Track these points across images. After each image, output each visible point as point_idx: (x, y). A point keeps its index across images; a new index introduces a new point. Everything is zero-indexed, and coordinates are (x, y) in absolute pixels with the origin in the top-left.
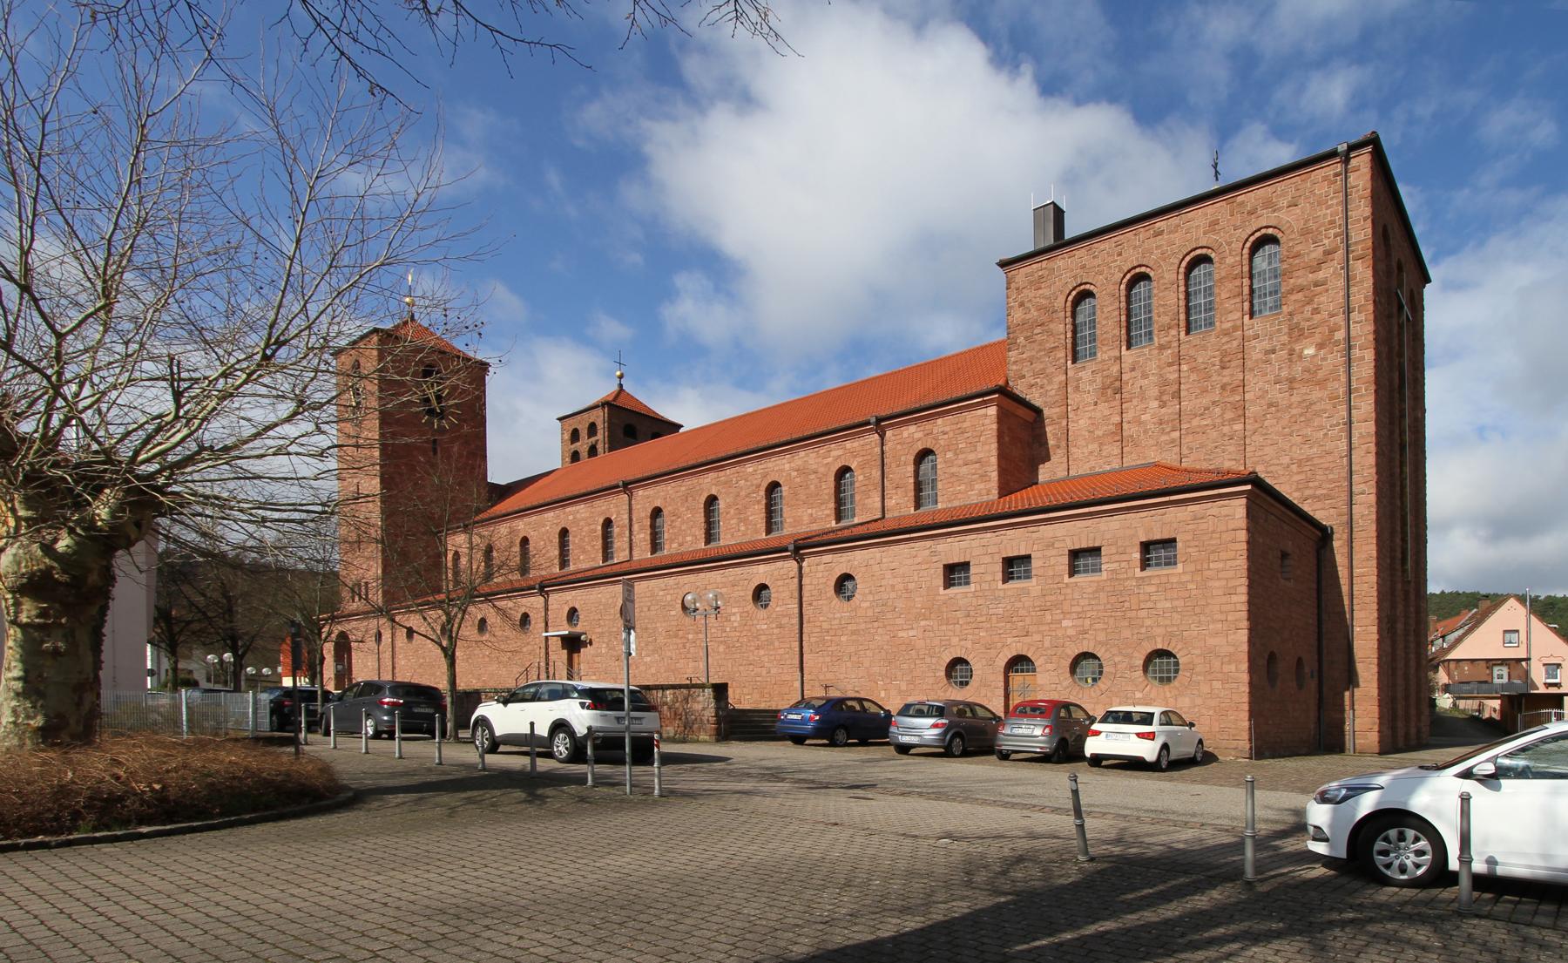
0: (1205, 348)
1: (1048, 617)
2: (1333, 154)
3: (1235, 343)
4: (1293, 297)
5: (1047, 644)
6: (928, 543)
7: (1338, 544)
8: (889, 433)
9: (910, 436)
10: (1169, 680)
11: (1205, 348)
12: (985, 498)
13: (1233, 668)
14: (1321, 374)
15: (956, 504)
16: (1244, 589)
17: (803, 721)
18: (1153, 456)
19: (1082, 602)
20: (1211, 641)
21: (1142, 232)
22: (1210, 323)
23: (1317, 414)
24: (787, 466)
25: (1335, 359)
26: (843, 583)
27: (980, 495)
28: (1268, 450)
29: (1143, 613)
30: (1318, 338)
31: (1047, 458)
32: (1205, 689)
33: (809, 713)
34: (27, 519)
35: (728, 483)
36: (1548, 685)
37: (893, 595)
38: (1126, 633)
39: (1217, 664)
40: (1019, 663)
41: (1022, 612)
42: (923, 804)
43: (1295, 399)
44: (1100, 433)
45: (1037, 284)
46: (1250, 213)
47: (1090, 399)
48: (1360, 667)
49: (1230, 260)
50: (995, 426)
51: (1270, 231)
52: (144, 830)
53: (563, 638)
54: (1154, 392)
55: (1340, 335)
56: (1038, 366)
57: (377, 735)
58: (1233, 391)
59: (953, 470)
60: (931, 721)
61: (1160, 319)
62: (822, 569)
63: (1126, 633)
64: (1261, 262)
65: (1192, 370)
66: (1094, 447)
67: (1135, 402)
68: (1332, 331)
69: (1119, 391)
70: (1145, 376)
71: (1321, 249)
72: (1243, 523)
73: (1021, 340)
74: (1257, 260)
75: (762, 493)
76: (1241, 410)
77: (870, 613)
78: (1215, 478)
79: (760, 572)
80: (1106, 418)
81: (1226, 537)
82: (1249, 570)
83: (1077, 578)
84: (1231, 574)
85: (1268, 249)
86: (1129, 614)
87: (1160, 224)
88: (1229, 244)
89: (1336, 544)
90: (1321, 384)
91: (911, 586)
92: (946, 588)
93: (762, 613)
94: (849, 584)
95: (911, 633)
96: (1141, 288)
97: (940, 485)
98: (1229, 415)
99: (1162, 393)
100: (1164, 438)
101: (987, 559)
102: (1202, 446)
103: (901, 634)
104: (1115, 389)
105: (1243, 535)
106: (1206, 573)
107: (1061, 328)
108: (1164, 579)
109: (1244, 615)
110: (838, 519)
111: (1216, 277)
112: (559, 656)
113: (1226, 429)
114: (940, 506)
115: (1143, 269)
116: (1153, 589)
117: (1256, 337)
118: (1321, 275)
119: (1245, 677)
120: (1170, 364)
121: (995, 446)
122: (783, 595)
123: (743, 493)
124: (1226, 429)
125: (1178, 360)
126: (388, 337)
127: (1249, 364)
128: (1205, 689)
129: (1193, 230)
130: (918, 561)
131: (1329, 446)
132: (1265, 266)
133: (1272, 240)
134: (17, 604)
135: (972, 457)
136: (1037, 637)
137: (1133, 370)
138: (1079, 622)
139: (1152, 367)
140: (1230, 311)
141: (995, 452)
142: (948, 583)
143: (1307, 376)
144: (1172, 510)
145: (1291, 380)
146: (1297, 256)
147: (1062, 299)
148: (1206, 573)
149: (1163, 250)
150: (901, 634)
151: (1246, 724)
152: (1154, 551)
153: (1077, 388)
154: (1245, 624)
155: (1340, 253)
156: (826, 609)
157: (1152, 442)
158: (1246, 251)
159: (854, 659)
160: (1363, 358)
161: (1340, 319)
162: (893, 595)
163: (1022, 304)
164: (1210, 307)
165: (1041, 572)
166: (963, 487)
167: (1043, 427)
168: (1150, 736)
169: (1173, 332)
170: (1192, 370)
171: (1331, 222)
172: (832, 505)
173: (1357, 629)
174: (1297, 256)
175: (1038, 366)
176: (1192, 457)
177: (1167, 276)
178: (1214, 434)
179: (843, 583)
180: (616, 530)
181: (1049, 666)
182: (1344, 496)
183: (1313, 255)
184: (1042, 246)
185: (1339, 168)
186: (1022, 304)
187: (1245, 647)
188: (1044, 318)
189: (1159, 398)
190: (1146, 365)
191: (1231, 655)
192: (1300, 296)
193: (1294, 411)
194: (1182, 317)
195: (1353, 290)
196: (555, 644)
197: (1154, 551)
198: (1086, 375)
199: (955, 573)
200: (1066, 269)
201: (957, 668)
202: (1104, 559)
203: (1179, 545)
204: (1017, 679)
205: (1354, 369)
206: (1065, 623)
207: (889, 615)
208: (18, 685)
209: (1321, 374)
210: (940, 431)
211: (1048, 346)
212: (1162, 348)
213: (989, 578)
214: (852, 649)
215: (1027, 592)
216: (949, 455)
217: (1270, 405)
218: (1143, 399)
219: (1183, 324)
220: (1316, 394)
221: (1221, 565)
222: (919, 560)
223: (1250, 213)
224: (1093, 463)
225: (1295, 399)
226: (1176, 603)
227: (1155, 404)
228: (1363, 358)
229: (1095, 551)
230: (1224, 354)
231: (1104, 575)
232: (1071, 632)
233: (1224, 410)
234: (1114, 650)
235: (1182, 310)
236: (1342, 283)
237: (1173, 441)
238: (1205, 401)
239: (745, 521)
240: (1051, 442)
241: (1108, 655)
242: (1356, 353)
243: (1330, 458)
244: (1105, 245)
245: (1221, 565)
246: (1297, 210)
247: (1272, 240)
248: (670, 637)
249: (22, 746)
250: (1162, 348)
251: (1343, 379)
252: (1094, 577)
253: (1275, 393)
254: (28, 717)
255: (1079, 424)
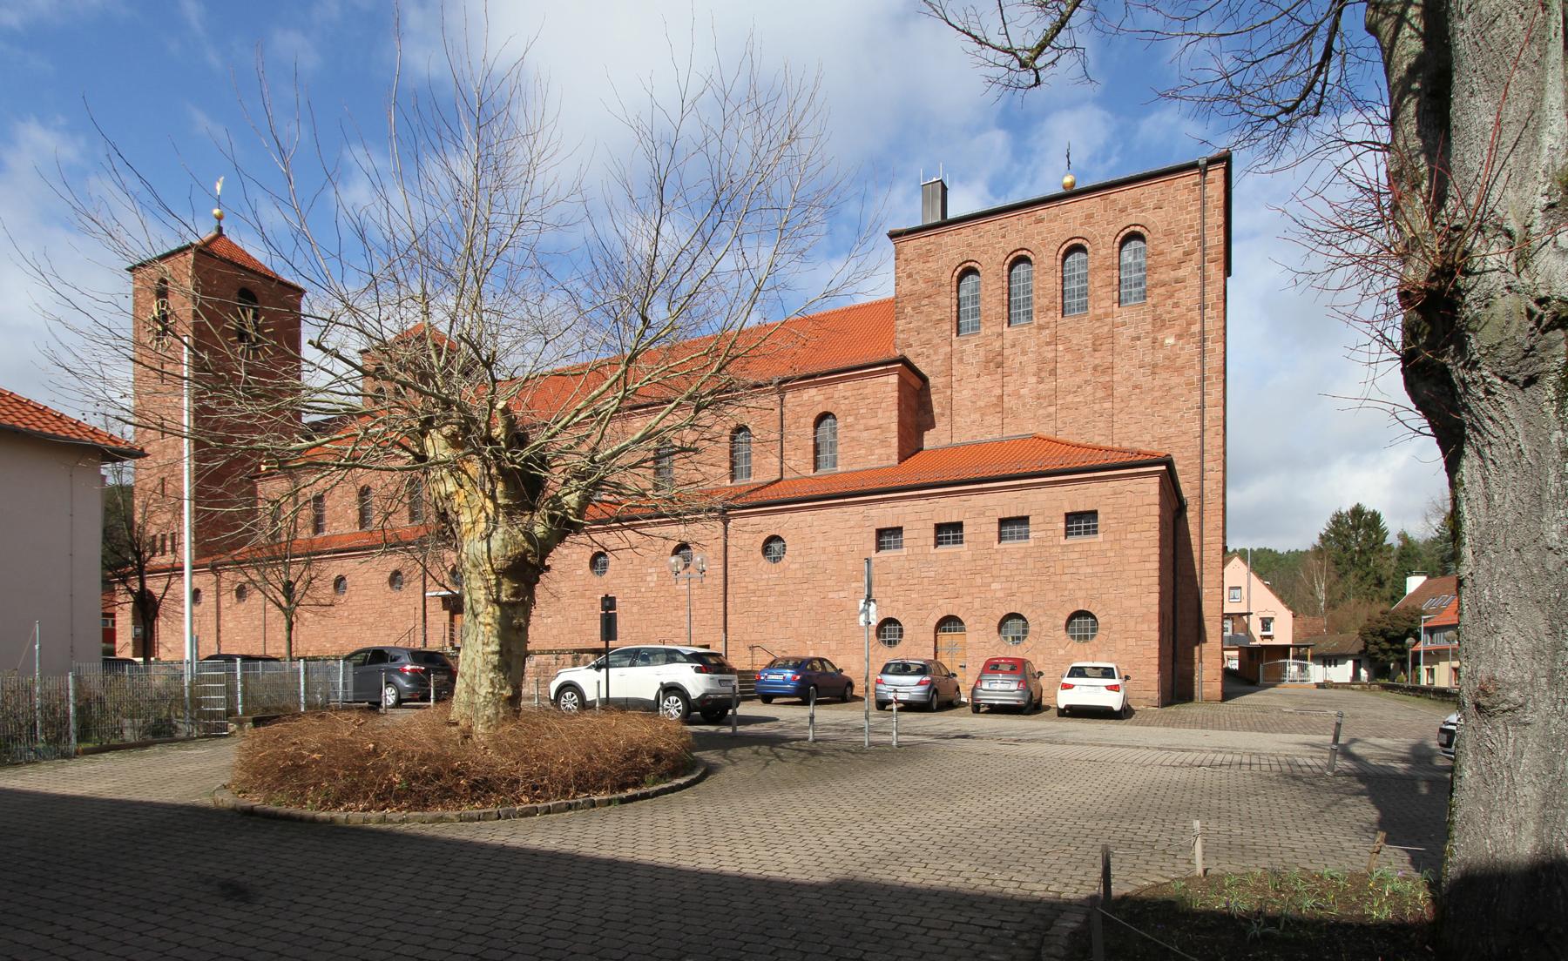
0: (1078, 331)
1: (979, 581)
2: (1194, 166)
3: (1106, 329)
4: (1157, 291)
5: (977, 604)
6: (861, 508)
7: (1191, 515)
8: (788, 396)
9: (813, 398)
10: (1086, 637)
11: (1078, 331)
12: (885, 463)
13: (1145, 627)
14: (1179, 363)
15: (856, 467)
16: (1156, 558)
17: (785, 681)
18: (1031, 428)
19: (1011, 567)
20: (1127, 603)
21: (1024, 218)
22: (1084, 307)
23: (1175, 398)
25: (1191, 349)
26: (771, 546)
27: (880, 459)
28: (1133, 427)
29: (1066, 578)
30: (1177, 330)
31: (932, 425)
32: (1121, 646)
33: (789, 674)
34: (506, 506)
36: (1264, 637)
37: (824, 557)
38: (1051, 596)
39: (1131, 624)
40: (949, 623)
41: (953, 576)
42: (1046, 747)
43: (1158, 382)
44: (981, 404)
45: (926, 256)
46: (1122, 211)
47: (973, 371)
48: (1207, 624)
49: (1103, 252)
50: (896, 394)
51: (1138, 229)
52: (681, 781)
53: (444, 598)
54: (1033, 368)
55: (1196, 328)
56: (924, 337)
57: (399, 703)
58: (1103, 372)
59: (854, 434)
60: (917, 679)
61: (1040, 302)
62: (750, 530)
63: (1051, 596)
64: (1128, 256)
65: (1067, 350)
66: (976, 416)
67: (1015, 376)
68: (1189, 324)
69: (1000, 365)
70: (1024, 353)
71: (1181, 251)
72: (1156, 499)
73: (909, 309)
74: (1125, 253)
76: (1109, 389)
77: (799, 575)
78: (1125, 458)
80: (989, 390)
81: (1142, 511)
82: (1161, 540)
83: (1006, 544)
84: (1145, 543)
85: (1134, 244)
86: (1055, 578)
87: (1041, 212)
88: (1102, 237)
89: (1189, 515)
90: (1179, 370)
91: (843, 549)
92: (877, 551)
94: (776, 546)
95: (842, 594)
96: (1021, 269)
97: (839, 448)
98: (1100, 394)
99: (1040, 370)
100: (1041, 412)
101: (920, 525)
102: (1075, 420)
103: (831, 595)
104: (996, 362)
105: (1156, 510)
106: (1124, 543)
107: (947, 300)
108: (1086, 547)
109: (1156, 580)
110: (733, 478)
111: (1090, 266)
112: (439, 617)
113: (1097, 407)
114: (839, 469)
115: (1024, 253)
116: (1075, 556)
117: (1124, 324)
118: (1181, 273)
119: (1156, 635)
120: (1048, 344)
121: (896, 413)
122: (706, 557)
124: (1097, 407)
125: (1054, 340)
126: (204, 252)
127: (1117, 348)
128: (1121, 646)
129: (1071, 220)
130: (853, 524)
131: (1185, 426)
132: (1130, 259)
133: (1139, 237)
134: (499, 584)
135: (873, 422)
136: (969, 599)
137: (1013, 346)
138: (1007, 585)
139: (1031, 344)
140: (1102, 299)
141: (896, 419)
142: (880, 547)
143: (1167, 363)
144: (1094, 485)
145: (1155, 366)
146: (1162, 253)
148: (1124, 543)
149: (1043, 234)
150: (831, 595)
151: (1156, 676)
152: (1081, 521)
153: (961, 360)
154: (1156, 588)
155: (1197, 255)
156: (751, 567)
157: (1030, 415)
158: (1117, 245)
159: (782, 619)
160: (1214, 350)
161: (1196, 314)
162: (824, 557)
163: (910, 276)
164: (1083, 292)
165: (972, 538)
166: (863, 452)
167: (929, 395)
168: (1115, 688)
169: (1052, 314)
170: (1067, 350)
171: (1191, 227)
172: (728, 464)
173: (1205, 591)
174: (1162, 253)
175: (924, 337)
176: (1066, 431)
177: (1046, 258)
178: (1085, 411)
179: (771, 546)
181: (979, 626)
182: (1197, 472)
183: (1175, 255)
184: (930, 221)
185: (1197, 178)
186: (910, 276)
187: (1156, 609)
188: (930, 291)
189: (1037, 374)
190: (1024, 342)
191: (1144, 616)
192: (1162, 290)
193: (1157, 394)
194: (1059, 300)
195: (1207, 289)
196: (435, 607)
197: (1081, 521)
198: (971, 349)
199: (887, 536)
200: (953, 247)
202: (1031, 528)
203: (1100, 517)
204: (945, 638)
205: (1207, 360)
206: (994, 586)
207: (819, 577)
208: (496, 658)
209: (1179, 363)
210: (840, 395)
211: (935, 317)
212: (1041, 327)
213: (921, 543)
214: (781, 610)
215: (958, 557)
216: (850, 420)
217: (1135, 387)
218: (1022, 374)
219: (1059, 306)
220: (1175, 380)
221: (1135, 536)
222: (852, 523)
223: (1122, 211)
224: (974, 432)
225: (1158, 382)
226: (1096, 569)
227: (1034, 380)
228: (1214, 350)
229: (1023, 520)
230: (1096, 338)
231: (1031, 542)
232: (1000, 594)
233: (1095, 389)
234: (1039, 611)
235: (1059, 294)
236: (1197, 282)
237: (1049, 415)
238: (1078, 380)
240: (936, 410)
241: (1033, 616)
242: (1209, 345)
243: (1185, 438)
244: (991, 227)
245: (1135, 536)
246: (1161, 213)
247: (1139, 237)
248: (575, 597)
249: (497, 714)
250: (1041, 327)
251: (1198, 367)
252: (1022, 544)
253: (1141, 377)
254: (502, 688)
255: (963, 394)
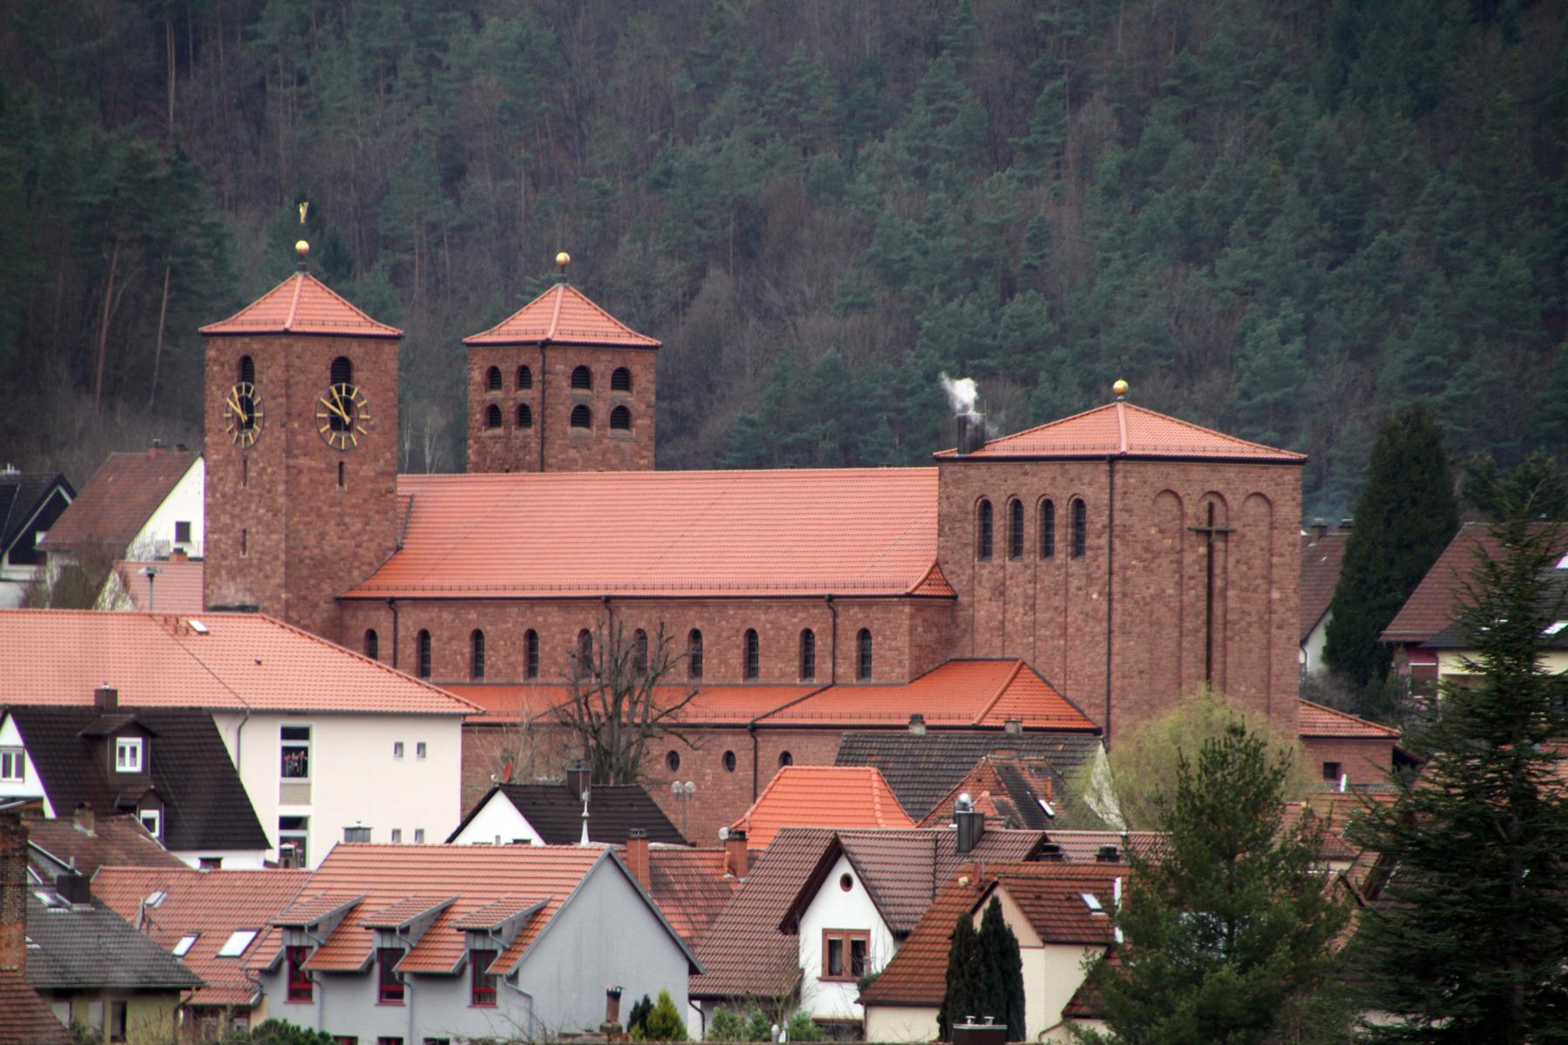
11: (1050, 573)
24: (763, 617)
35: (711, 620)
36: (122, 750)
69: (1002, 594)
75: (741, 638)
79: (729, 742)
93: (729, 776)
123: (724, 634)
147: (971, 504)
180: (818, 642)
198: (987, 571)
201: (396, 833)
239: (725, 662)
